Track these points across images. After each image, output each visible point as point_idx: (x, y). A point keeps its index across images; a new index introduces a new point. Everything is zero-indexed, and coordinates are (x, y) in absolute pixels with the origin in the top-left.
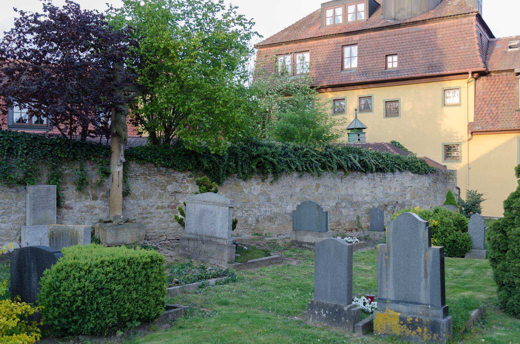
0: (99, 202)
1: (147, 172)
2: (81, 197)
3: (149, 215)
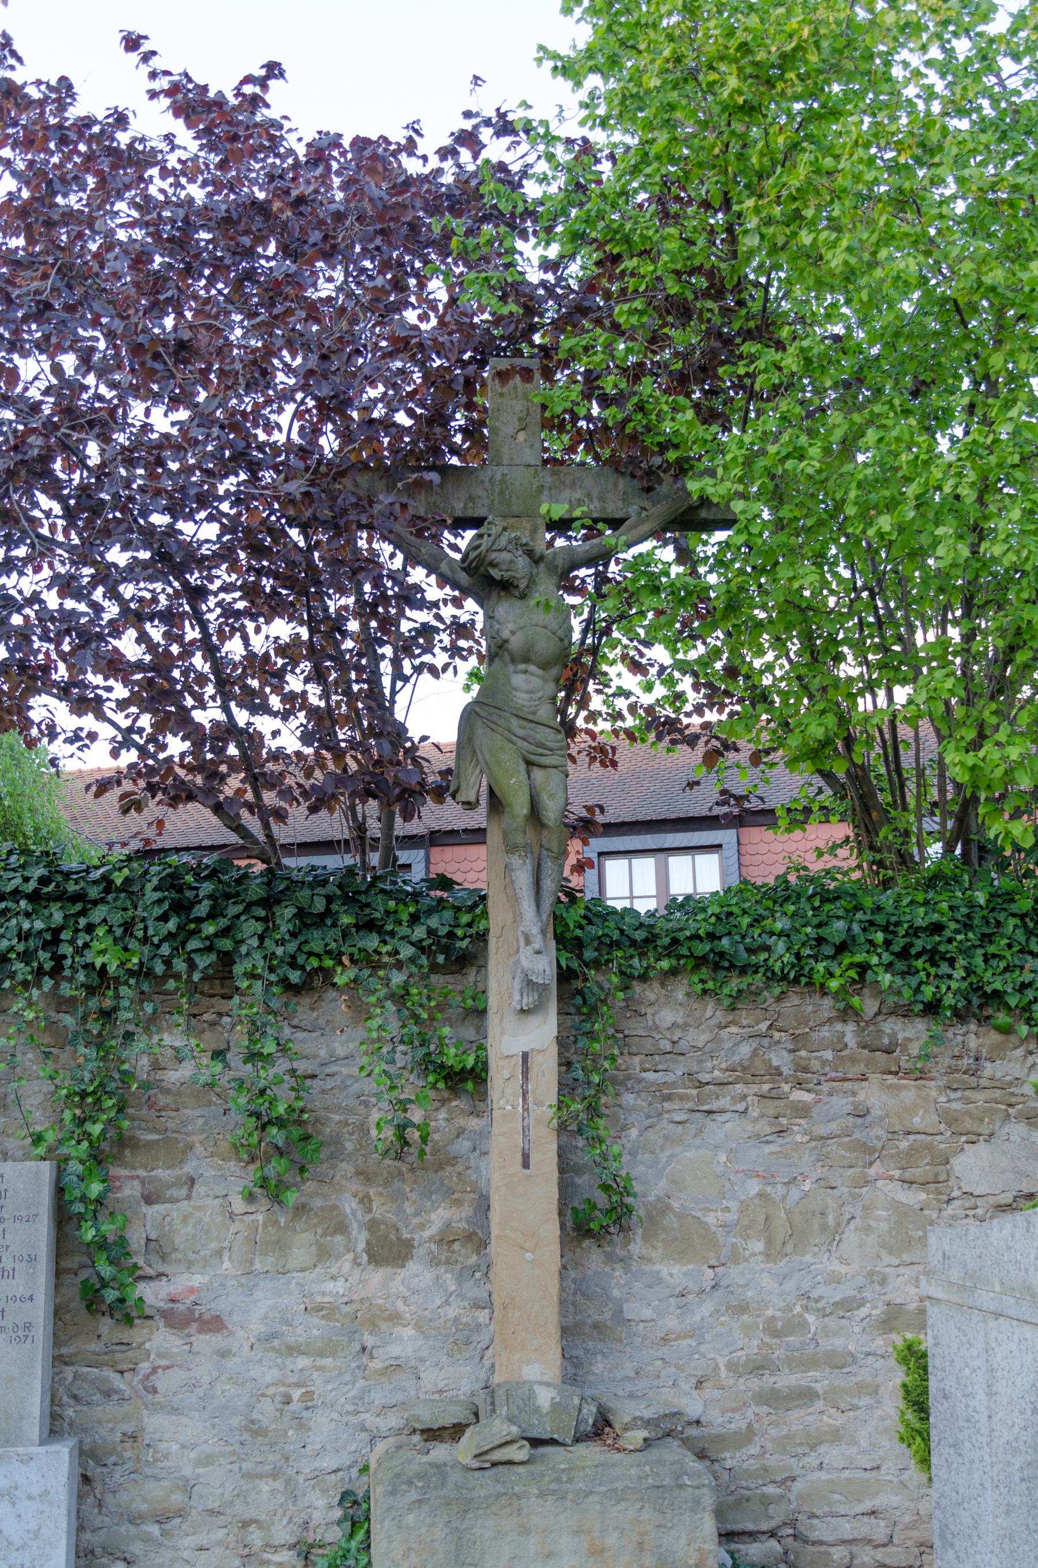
0: (417, 1274)
1: (779, 1058)
2: (281, 1246)
3: (820, 1380)
